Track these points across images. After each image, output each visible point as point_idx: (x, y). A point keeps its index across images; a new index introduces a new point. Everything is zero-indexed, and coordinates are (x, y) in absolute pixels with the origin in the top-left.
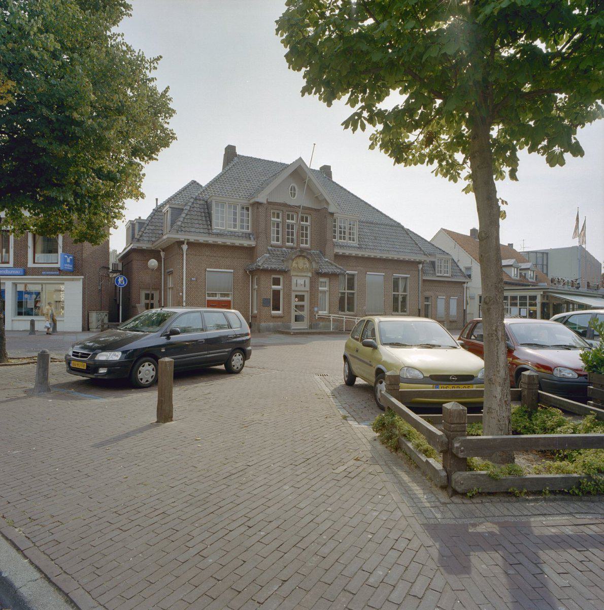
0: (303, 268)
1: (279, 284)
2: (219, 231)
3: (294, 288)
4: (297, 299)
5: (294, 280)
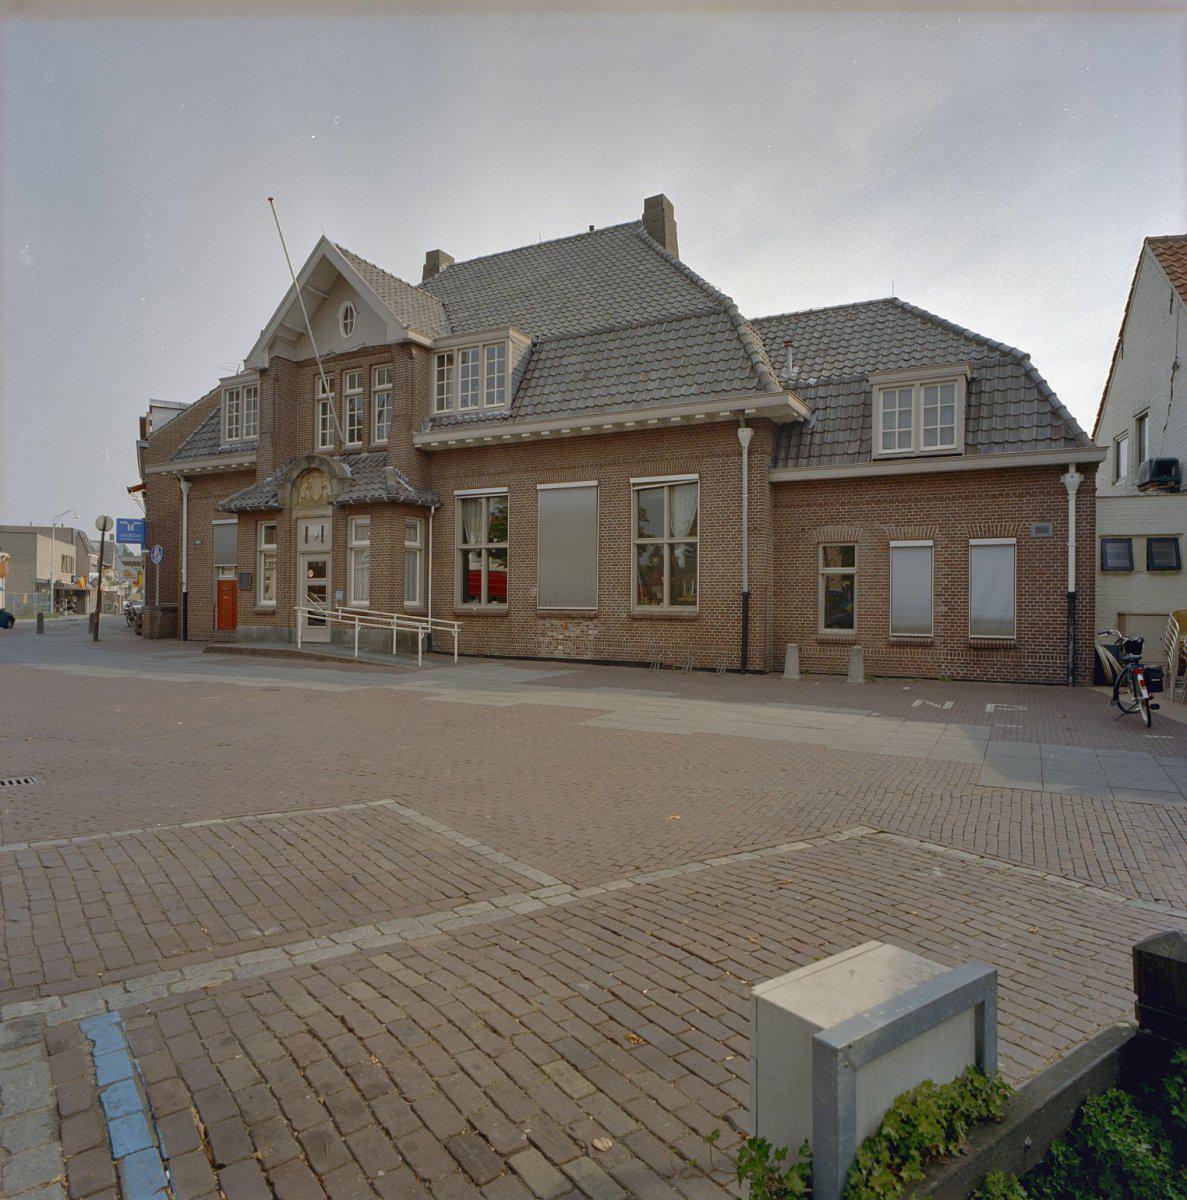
3: (301, 546)
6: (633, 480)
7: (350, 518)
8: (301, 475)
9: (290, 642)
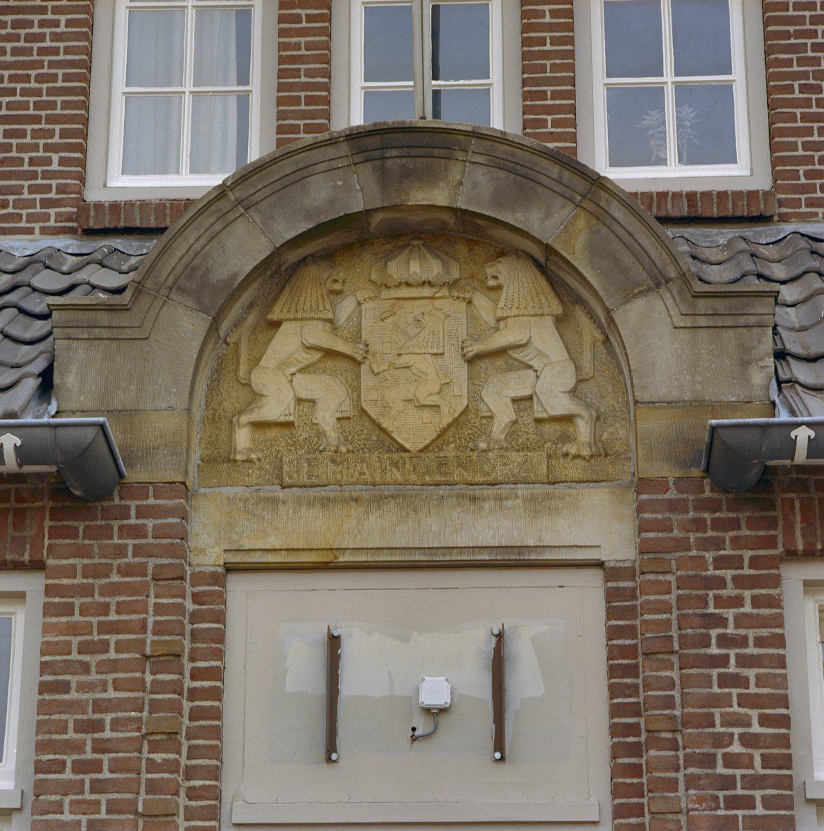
0: (465, 426)
5: (270, 636)
8: (279, 272)
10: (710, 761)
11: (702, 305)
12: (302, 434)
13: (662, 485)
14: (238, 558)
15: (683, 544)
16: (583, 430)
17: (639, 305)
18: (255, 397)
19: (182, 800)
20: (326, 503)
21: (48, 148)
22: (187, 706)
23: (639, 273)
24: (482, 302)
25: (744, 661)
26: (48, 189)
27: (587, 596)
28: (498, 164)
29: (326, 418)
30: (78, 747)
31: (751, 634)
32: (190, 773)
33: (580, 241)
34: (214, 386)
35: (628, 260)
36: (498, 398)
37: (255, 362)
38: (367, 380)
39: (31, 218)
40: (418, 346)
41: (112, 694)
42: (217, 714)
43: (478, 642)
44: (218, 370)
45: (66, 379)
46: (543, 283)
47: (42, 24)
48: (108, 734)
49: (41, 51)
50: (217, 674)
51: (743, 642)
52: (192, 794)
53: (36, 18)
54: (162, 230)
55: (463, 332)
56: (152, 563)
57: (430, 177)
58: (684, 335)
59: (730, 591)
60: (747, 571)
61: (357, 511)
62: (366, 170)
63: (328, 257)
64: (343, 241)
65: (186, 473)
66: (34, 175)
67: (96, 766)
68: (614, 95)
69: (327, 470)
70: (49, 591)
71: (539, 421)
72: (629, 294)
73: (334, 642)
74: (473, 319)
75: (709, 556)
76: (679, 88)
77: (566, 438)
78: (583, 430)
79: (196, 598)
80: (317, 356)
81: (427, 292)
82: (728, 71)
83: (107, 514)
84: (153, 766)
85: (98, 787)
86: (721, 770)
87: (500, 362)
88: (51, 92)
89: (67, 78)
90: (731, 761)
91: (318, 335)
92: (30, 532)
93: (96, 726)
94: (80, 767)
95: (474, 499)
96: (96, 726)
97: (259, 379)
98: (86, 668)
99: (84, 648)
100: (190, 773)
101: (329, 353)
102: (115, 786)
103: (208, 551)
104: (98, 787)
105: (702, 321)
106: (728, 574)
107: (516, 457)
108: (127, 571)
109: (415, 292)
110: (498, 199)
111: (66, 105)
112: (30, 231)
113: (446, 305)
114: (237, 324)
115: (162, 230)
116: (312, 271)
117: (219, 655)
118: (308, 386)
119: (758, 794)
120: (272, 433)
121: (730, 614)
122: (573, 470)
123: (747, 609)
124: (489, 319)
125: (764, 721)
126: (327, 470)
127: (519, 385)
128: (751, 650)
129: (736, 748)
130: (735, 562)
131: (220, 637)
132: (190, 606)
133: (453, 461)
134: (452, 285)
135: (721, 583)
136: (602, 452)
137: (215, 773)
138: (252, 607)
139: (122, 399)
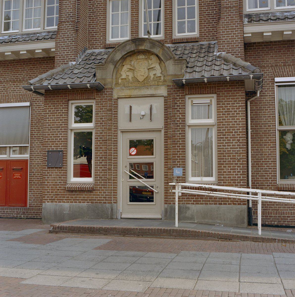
0: (148, 77)
1: (89, 120)
2: (6, 37)
3: (123, 123)
4: (134, 151)
5: (123, 107)
6: (277, 79)
7: (71, 102)
8: (124, 58)
9: (112, 218)
10: (175, 121)
11: (176, 61)
12: (127, 80)
13: (170, 86)
14: (118, 97)
15: (173, 94)
16: (162, 78)
17: (168, 62)
18: (121, 75)
19: (113, 127)
20: (129, 89)
21: (101, 36)
22: (113, 115)
23: (168, 57)
24: (150, 61)
25: (179, 108)
26: (101, 42)
27: (162, 100)
28: (150, 43)
29: (130, 78)
30: (100, 121)
31: (181, 105)
32: (114, 124)
33: (161, 53)
34: (116, 74)
35: (167, 55)
36: (152, 74)
37: (121, 70)
38: (135, 72)
39: (99, 46)
40: (142, 68)
41: (104, 115)
42: (117, 116)
43: (149, 106)
44: (117, 72)
45: (97, 75)
46: (157, 58)
47: (99, 18)
48: (103, 119)
49: (99, 22)
50: (117, 111)
51: (180, 106)
52: (114, 126)
53: (98, 17)
54: (114, 48)
55: (147, 65)
56: (108, 98)
57: (142, 45)
58: (174, 65)
59: (178, 99)
60: (180, 97)
61: (133, 90)
62: (134, 44)
63: (130, 56)
64: (132, 54)
65: (112, 86)
66: (99, 40)
67: (102, 123)
68: (179, 23)
69: (130, 85)
70: (96, 102)
71: (157, 77)
72: (167, 61)
73: (131, 107)
74: (149, 63)
75: (176, 95)
76: (188, 21)
77: (160, 79)
78: (162, 78)
79: (114, 102)
80: (129, 69)
81: (143, 60)
82: (195, 18)
83: (103, 92)
84: (109, 123)
85: (103, 126)
86: (176, 122)
87: (152, 69)
88: (101, 28)
89: (103, 26)
90: (177, 121)
91: (129, 67)
92: (93, 95)
93: (102, 119)
94: (101, 123)
95: (148, 88)
96: (102, 119)
97: (121, 73)
98: (100, 111)
99: (101, 109)
100: (114, 124)
101: (130, 69)
102: (104, 126)
103: (115, 96)
104: (103, 126)
105: (176, 64)
106: (178, 97)
107: (154, 82)
108: (105, 99)
109: (141, 60)
110: (151, 48)
111: (103, 30)
112: (99, 48)
113: (145, 62)
114: (119, 66)
115: (114, 48)
116: (128, 58)
117: (117, 109)
118: (128, 73)
119: (180, 125)
120: (124, 80)
121: (178, 102)
122: (161, 84)
123: (180, 102)
124: (151, 63)
125: (182, 116)
126: (130, 85)
127: (154, 72)
128: (181, 107)
129: (178, 119)
130: (179, 96)
131: (117, 107)
132: (113, 103)
133: (146, 83)
134: (146, 59)
135: (177, 98)
136: (165, 81)
137: (117, 124)
138: (121, 103)
139: (104, 77)
